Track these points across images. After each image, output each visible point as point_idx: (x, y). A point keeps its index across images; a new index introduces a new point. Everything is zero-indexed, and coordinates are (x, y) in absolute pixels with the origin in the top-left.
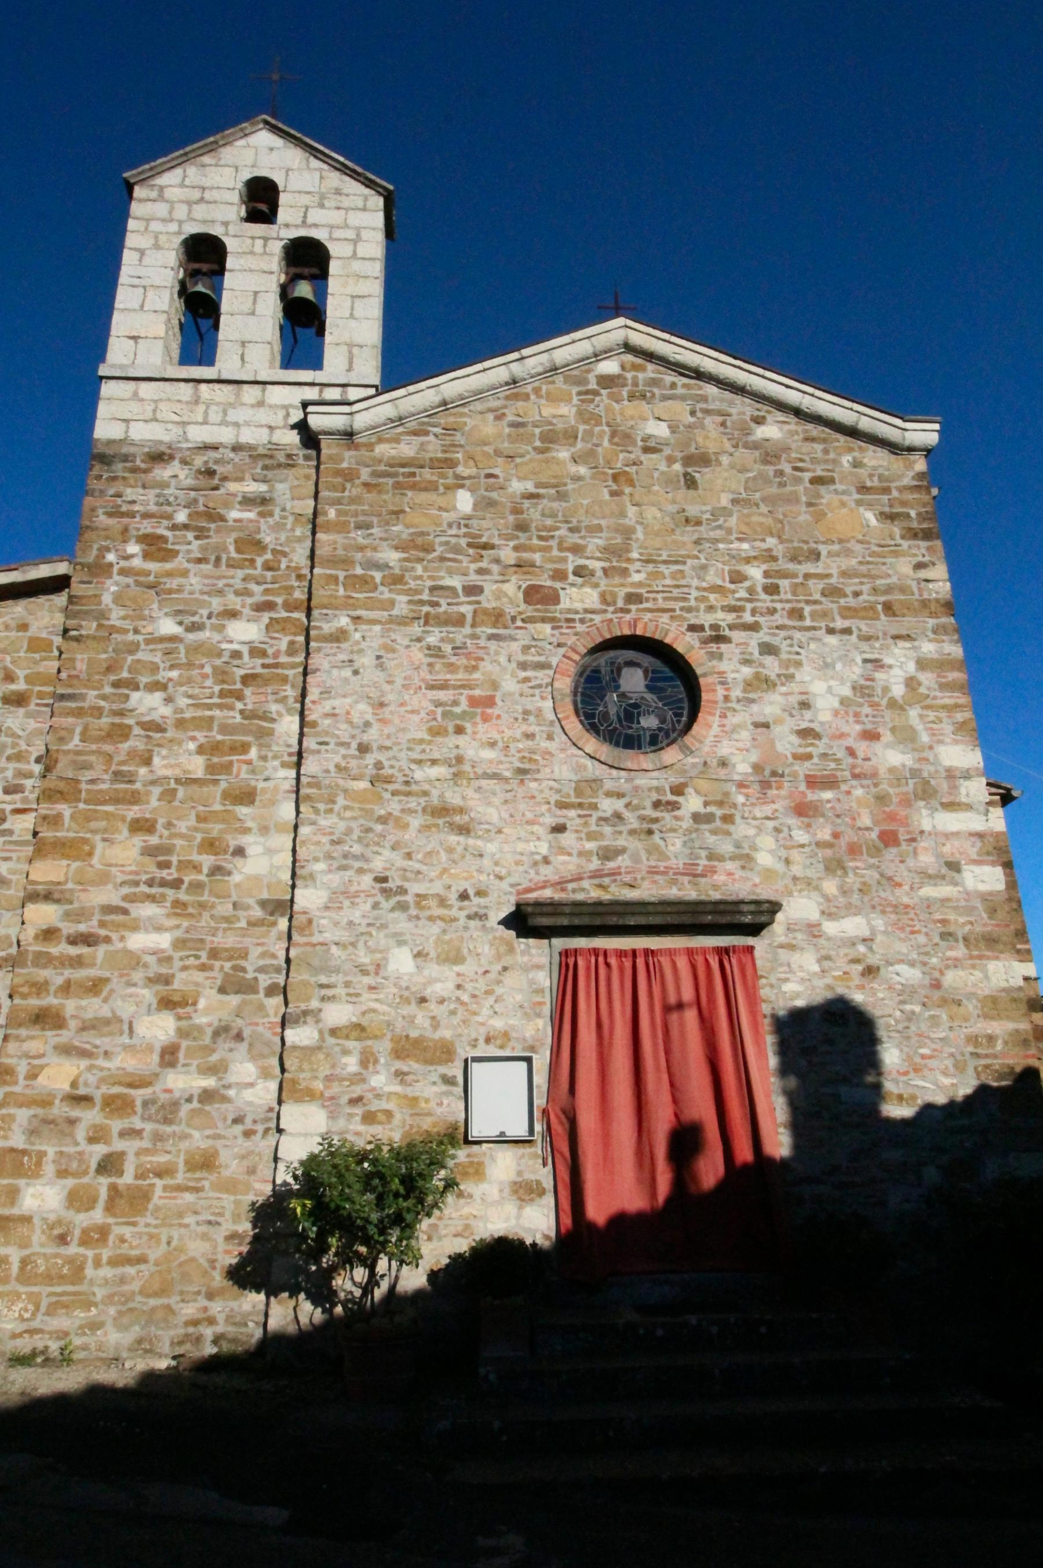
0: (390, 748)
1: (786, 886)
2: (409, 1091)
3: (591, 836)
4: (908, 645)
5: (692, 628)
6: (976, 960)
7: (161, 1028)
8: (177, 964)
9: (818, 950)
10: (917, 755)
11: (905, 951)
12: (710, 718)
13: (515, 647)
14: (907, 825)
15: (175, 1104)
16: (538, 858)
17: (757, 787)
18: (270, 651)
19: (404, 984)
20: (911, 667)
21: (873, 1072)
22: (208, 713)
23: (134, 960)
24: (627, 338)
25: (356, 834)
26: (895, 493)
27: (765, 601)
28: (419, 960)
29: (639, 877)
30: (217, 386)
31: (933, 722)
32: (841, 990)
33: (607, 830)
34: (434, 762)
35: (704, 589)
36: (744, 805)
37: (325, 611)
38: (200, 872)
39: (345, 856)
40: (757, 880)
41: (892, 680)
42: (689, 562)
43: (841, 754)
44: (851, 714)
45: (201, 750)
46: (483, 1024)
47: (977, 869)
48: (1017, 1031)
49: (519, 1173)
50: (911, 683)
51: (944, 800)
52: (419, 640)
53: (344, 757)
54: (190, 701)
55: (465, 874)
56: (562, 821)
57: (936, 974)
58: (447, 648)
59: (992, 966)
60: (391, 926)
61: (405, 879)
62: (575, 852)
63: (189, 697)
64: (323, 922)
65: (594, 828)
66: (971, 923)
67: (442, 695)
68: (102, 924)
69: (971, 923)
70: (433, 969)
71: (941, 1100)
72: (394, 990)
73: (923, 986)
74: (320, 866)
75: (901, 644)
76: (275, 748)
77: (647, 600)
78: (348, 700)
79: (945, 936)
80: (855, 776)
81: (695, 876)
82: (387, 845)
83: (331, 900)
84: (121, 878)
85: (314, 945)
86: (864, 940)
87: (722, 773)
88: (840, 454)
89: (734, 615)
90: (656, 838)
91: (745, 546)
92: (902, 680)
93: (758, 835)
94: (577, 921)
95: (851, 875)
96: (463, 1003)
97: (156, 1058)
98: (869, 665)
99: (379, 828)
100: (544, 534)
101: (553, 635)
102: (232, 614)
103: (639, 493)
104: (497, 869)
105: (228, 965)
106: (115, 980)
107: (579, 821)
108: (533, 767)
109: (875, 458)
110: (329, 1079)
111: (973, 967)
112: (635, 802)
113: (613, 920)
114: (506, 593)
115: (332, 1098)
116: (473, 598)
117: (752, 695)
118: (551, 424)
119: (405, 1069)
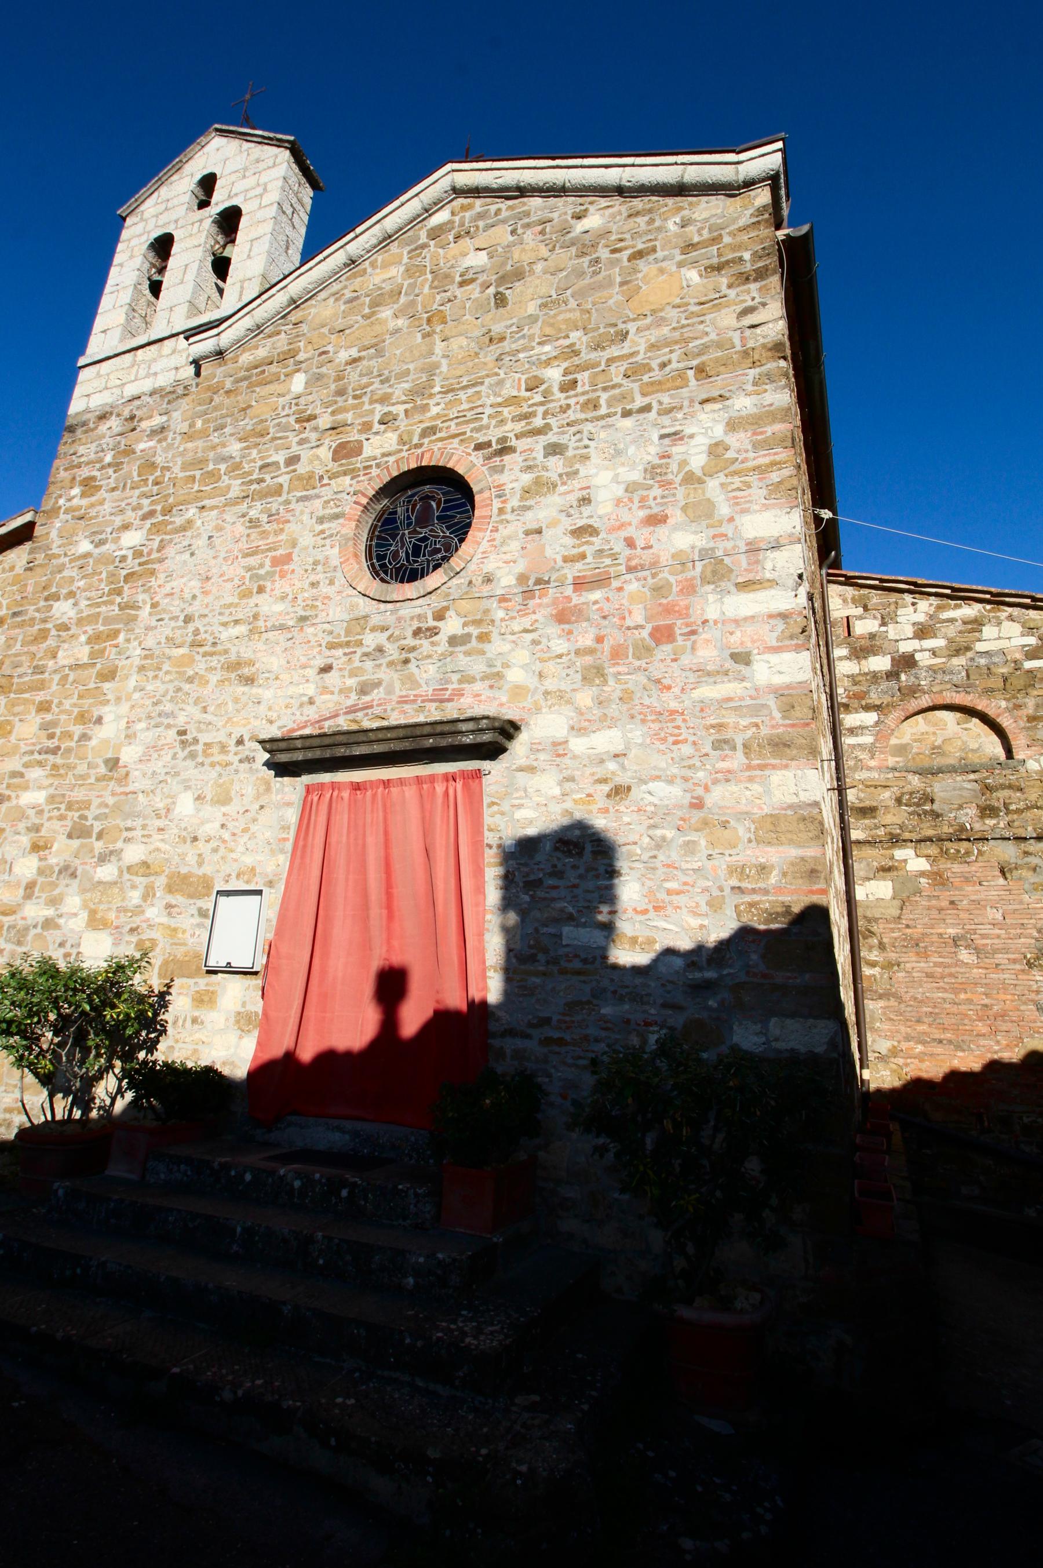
0: (206, 615)
1: (536, 703)
2: (173, 923)
3: (353, 674)
4: (717, 406)
5: (478, 447)
6: (755, 770)
7: (27, 867)
8: (46, 815)
9: (561, 771)
10: (712, 532)
11: (663, 765)
12: (480, 534)
13: (317, 503)
14: (688, 616)
15: (27, 929)
16: (305, 699)
17: (519, 599)
18: (146, 551)
19: (183, 825)
20: (719, 431)
21: (605, 909)
22: (98, 610)
23: (21, 814)
24: (453, 181)
25: (171, 693)
26: (727, 240)
27: (559, 400)
28: (198, 802)
29: (389, 708)
30: (148, 348)
31: (739, 489)
32: (579, 814)
33: (369, 664)
34: (236, 622)
35: (500, 405)
36: (502, 620)
37: (181, 507)
38: (72, 739)
39: (160, 715)
40: (504, 699)
41: (692, 451)
42: (487, 381)
43: (619, 547)
44: (636, 501)
45: (89, 641)
46: (236, 860)
47: (774, 659)
48: (802, 859)
49: (244, 1004)
50: (716, 449)
51: (740, 580)
52: (243, 516)
53: (173, 629)
54: (89, 603)
55: (243, 722)
56: (329, 661)
57: (700, 791)
58: (264, 518)
59: (776, 777)
60: (182, 773)
61: (199, 731)
62: (336, 690)
63: (89, 599)
64: (137, 773)
65: (357, 664)
66: (757, 725)
67: (252, 561)
68: (8, 786)
69: (757, 725)
70: (208, 810)
71: (685, 944)
72: (176, 831)
73: (680, 807)
74: (142, 725)
75: (708, 407)
76: (137, 631)
77: (441, 430)
78: (183, 580)
79: (719, 745)
80: (630, 569)
81: (442, 701)
82: (191, 701)
83: (144, 754)
84: (24, 748)
85: (127, 794)
86: (616, 756)
87: (486, 590)
88: (666, 220)
89: (523, 423)
90: (412, 666)
91: (547, 348)
92: (705, 448)
93: (513, 650)
94: (310, 755)
95: (611, 682)
96: (224, 841)
97: (21, 892)
98: (667, 441)
99: (187, 687)
100: (358, 392)
101: (351, 485)
102: (126, 527)
103: (450, 328)
104: (270, 714)
105: (77, 814)
106: (8, 830)
107: (345, 659)
108: (313, 613)
109: (708, 209)
110: (119, 910)
111: (751, 779)
112: (397, 633)
113: (341, 751)
114: (319, 457)
115: (117, 927)
116: (292, 468)
117: (527, 503)
118: (380, 288)
119: (174, 902)
